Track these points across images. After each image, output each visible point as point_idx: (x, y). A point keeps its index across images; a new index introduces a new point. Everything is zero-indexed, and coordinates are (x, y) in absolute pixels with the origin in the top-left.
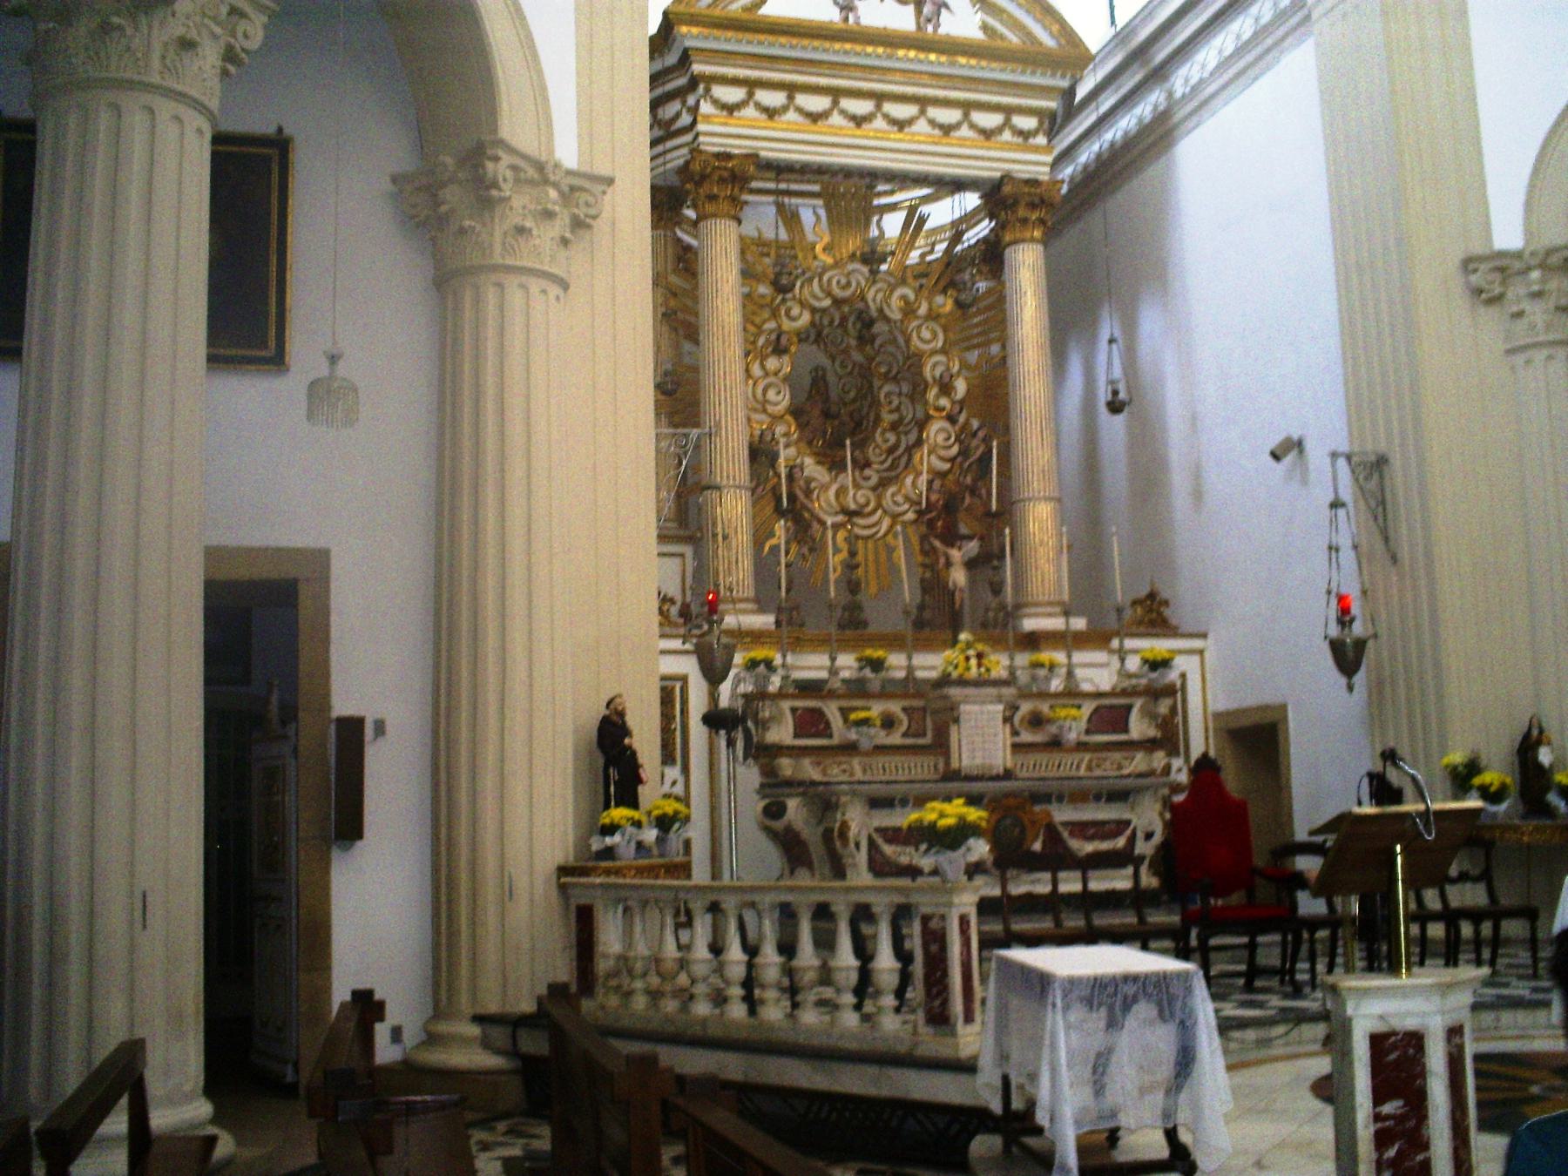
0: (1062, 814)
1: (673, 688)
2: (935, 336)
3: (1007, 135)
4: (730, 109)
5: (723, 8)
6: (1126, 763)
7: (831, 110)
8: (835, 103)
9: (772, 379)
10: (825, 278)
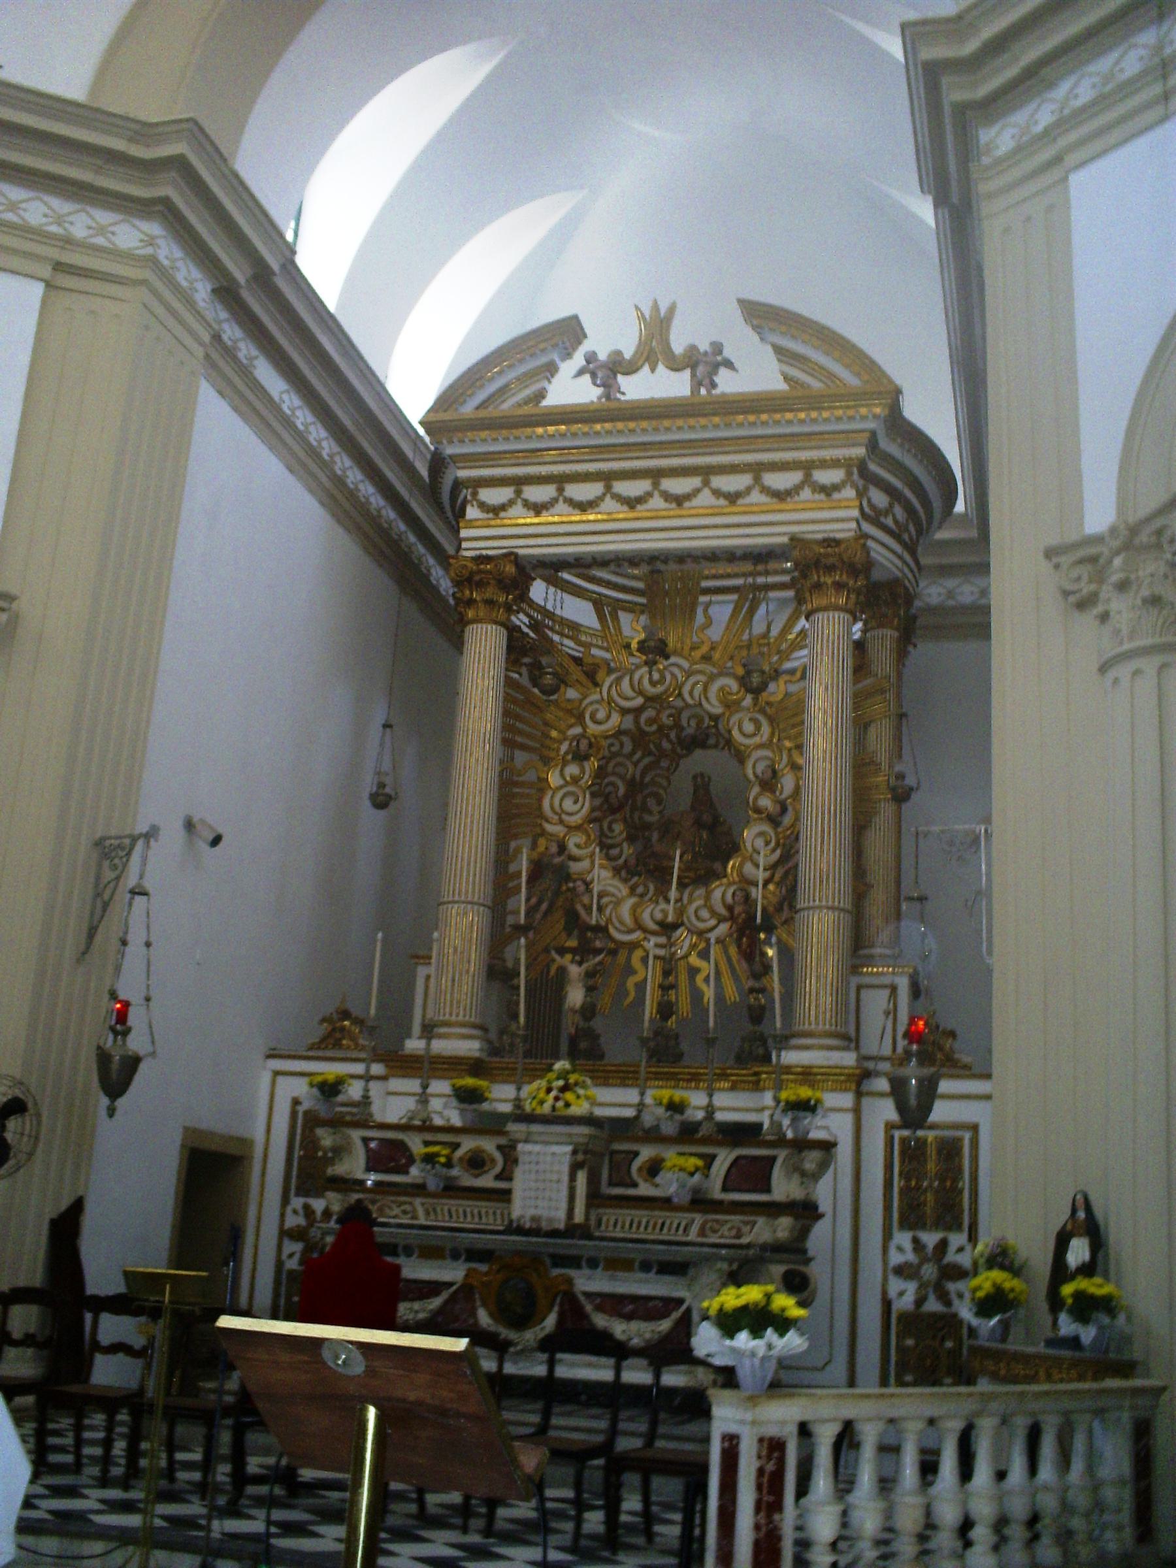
0: (587, 1282)
1: (960, 1140)
2: (758, 726)
3: (806, 494)
4: (496, 510)
5: (495, 408)
6: (746, 1229)
7: (604, 494)
8: (656, 485)
9: (571, 788)
10: (636, 677)
